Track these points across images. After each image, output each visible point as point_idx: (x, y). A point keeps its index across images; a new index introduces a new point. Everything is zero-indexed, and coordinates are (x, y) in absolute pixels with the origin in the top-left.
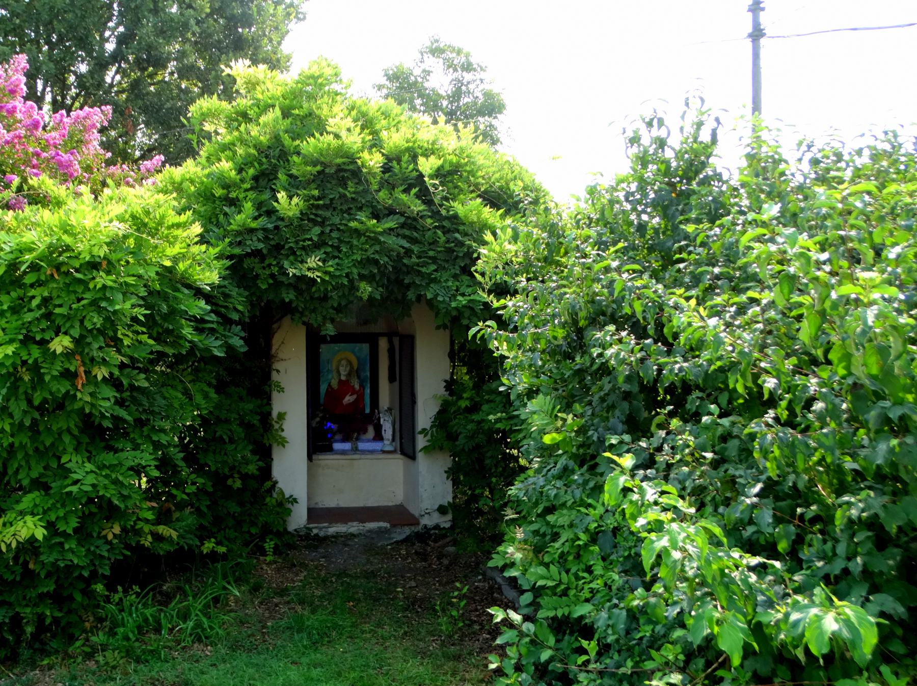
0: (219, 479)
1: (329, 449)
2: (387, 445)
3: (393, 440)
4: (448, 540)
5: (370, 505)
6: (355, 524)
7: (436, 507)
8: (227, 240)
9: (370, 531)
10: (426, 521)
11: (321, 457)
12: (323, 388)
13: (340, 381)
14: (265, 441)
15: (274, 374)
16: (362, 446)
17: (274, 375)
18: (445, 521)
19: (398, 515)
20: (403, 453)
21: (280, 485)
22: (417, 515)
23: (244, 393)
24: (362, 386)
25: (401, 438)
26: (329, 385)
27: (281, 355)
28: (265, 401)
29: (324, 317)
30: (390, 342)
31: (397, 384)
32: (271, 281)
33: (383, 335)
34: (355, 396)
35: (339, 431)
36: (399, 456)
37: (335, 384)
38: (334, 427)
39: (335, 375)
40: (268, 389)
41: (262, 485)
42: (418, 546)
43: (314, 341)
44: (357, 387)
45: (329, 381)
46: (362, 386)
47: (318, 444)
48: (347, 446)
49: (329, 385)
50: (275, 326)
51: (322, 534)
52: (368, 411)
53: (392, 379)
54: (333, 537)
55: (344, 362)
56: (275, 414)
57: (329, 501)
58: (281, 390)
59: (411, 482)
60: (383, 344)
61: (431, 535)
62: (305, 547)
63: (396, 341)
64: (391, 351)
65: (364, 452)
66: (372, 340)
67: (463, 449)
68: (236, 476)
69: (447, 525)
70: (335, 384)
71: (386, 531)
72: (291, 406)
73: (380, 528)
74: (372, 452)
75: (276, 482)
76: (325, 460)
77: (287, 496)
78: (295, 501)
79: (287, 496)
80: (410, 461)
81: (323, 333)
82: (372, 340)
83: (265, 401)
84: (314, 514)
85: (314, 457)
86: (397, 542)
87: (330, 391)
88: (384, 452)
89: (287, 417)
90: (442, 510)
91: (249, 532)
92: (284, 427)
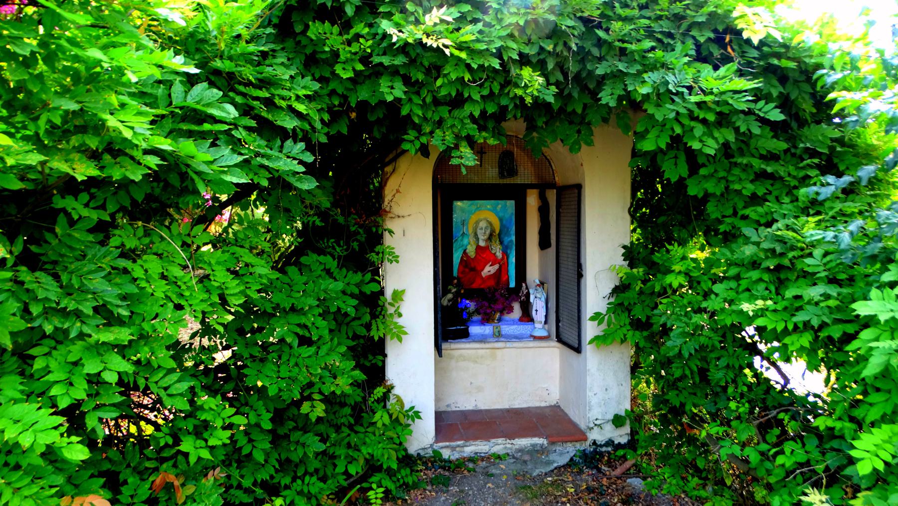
1: (464, 335)
2: (539, 329)
3: (546, 322)
4: (628, 464)
6: (500, 441)
8: (592, 495)
9: (520, 450)
10: (596, 435)
11: (453, 346)
12: (457, 257)
13: (478, 248)
16: (506, 329)
17: (388, 240)
18: (621, 436)
19: (552, 422)
20: (560, 340)
21: (396, 391)
22: (583, 426)
23: (332, 264)
24: (505, 254)
25: (558, 321)
26: (465, 252)
27: (396, 210)
29: (457, 136)
31: (552, 251)
32: (360, 67)
33: (532, 186)
34: (497, 267)
35: (477, 311)
36: (556, 344)
37: (471, 251)
38: (472, 306)
39: (472, 240)
41: (371, 393)
42: (587, 478)
44: (499, 255)
45: (464, 247)
46: (505, 254)
47: (450, 327)
48: (487, 329)
49: (465, 252)
50: (388, 169)
51: (455, 456)
52: (512, 284)
53: (544, 244)
54: (471, 460)
55: (483, 224)
56: (389, 293)
57: (466, 400)
58: (395, 259)
59: (574, 382)
60: (532, 201)
61: (602, 454)
62: (431, 482)
63: (552, 196)
64: (543, 211)
66: (517, 194)
68: (317, 396)
69: (624, 440)
70: (471, 251)
71: (542, 450)
72: (411, 277)
73: (533, 445)
74: (519, 338)
75: (392, 387)
76: (457, 349)
78: (417, 415)
80: (573, 354)
81: (454, 162)
82: (517, 194)
83: (368, 276)
84: (448, 423)
85: (445, 346)
87: (466, 260)
89: (407, 297)
90: (618, 421)
91: (346, 473)
92: (402, 310)
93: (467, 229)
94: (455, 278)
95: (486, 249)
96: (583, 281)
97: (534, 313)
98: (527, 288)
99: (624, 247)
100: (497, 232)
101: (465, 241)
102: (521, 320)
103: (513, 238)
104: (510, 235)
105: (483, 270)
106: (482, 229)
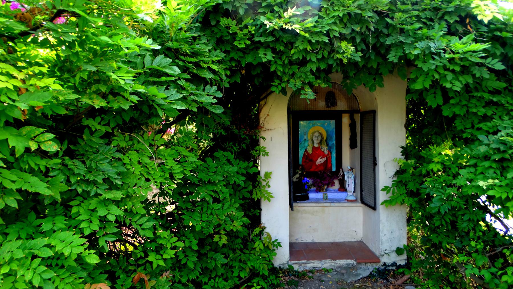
0: (205, 241)
1: (306, 198)
4: (405, 278)
5: (337, 241)
6: (328, 261)
7: (395, 248)
9: (340, 267)
12: (301, 153)
13: (314, 148)
14: (254, 196)
15: (261, 140)
16: (330, 195)
17: (262, 143)
18: (401, 260)
19: (359, 251)
20: (363, 202)
21: (267, 230)
22: (377, 254)
23: (231, 157)
24: (330, 151)
25: (362, 191)
26: (306, 150)
27: (267, 126)
28: (251, 164)
29: (303, 83)
30: (352, 119)
31: (358, 150)
33: (345, 112)
34: (325, 159)
35: (313, 185)
36: (360, 204)
37: (310, 150)
38: (310, 182)
39: (310, 143)
40: (254, 153)
43: (295, 117)
44: (326, 152)
45: (306, 147)
46: (330, 151)
47: (298, 194)
48: (320, 195)
49: (306, 150)
50: (262, 103)
51: (301, 269)
52: (334, 169)
53: (353, 146)
54: (310, 271)
55: (317, 134)
56: (262, 174)
57: (307, 237)
58: (267, 154)
59: (372, 227)
60: (346, 120)
61: (389, 271)
63: (357, 117)
64: (352, 126)
65: (333, 201)
66: (337, 117)
67: (439, 212)
68: (223, 232)
69: (403, 263)
70: (310, 150)
71: (353, 267)
73: (347, 264)
74: (338, 201)
77: (273, 239)
78: (279, 244)
79: (273, 239)
80: (371, 210)
81: (303, 96)
82: (337, 117)
83: (251, 164)
84: (297, 250)
85: (295, 204)
86: (363, 278)
87: (306, 155)
88: (348, 201)
89: (273, 176)
90: (399, 251)
91: (239, 276)
93: (307, 136)
94: (300, 165)
95: (319, 148)
96: (377, 167)
97: (347, 186)
98: (343, 171)
99: (402, 147)
100: (325, 138)
101: (306, 144)
102: (339, 190)
103: (334, 142)
104: (332, 141)
105: (317, 160)
106: (316, 137)
